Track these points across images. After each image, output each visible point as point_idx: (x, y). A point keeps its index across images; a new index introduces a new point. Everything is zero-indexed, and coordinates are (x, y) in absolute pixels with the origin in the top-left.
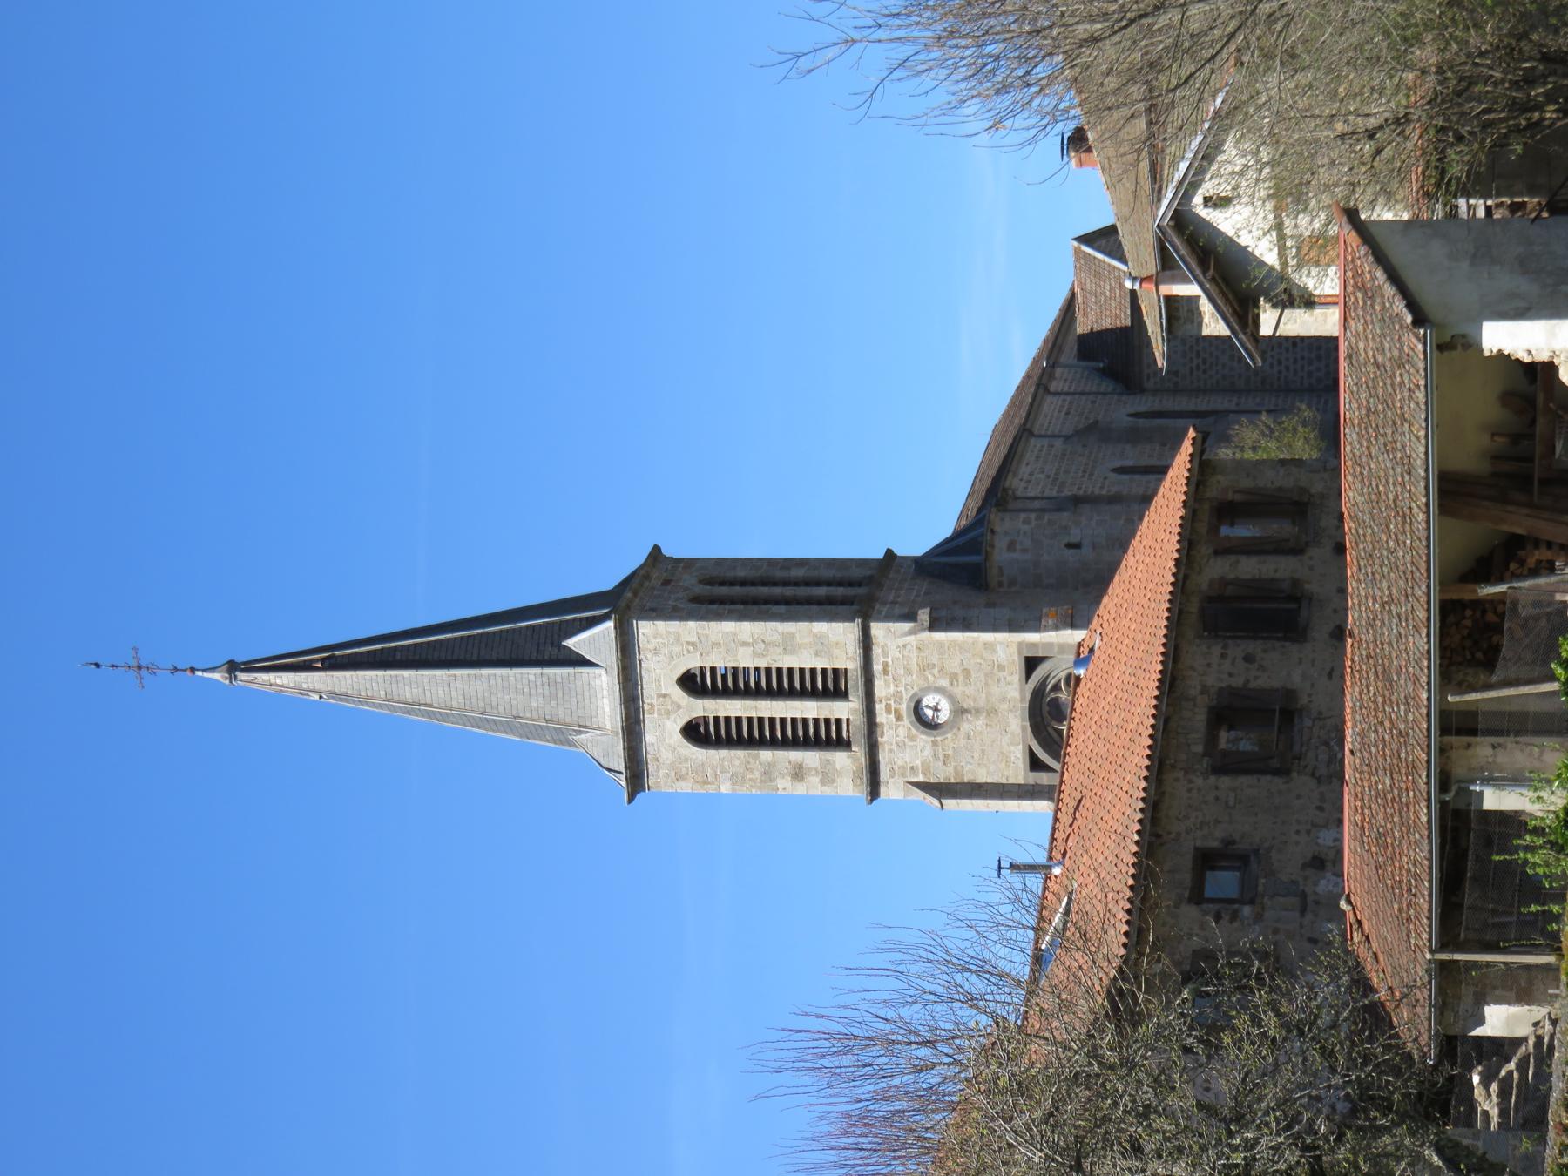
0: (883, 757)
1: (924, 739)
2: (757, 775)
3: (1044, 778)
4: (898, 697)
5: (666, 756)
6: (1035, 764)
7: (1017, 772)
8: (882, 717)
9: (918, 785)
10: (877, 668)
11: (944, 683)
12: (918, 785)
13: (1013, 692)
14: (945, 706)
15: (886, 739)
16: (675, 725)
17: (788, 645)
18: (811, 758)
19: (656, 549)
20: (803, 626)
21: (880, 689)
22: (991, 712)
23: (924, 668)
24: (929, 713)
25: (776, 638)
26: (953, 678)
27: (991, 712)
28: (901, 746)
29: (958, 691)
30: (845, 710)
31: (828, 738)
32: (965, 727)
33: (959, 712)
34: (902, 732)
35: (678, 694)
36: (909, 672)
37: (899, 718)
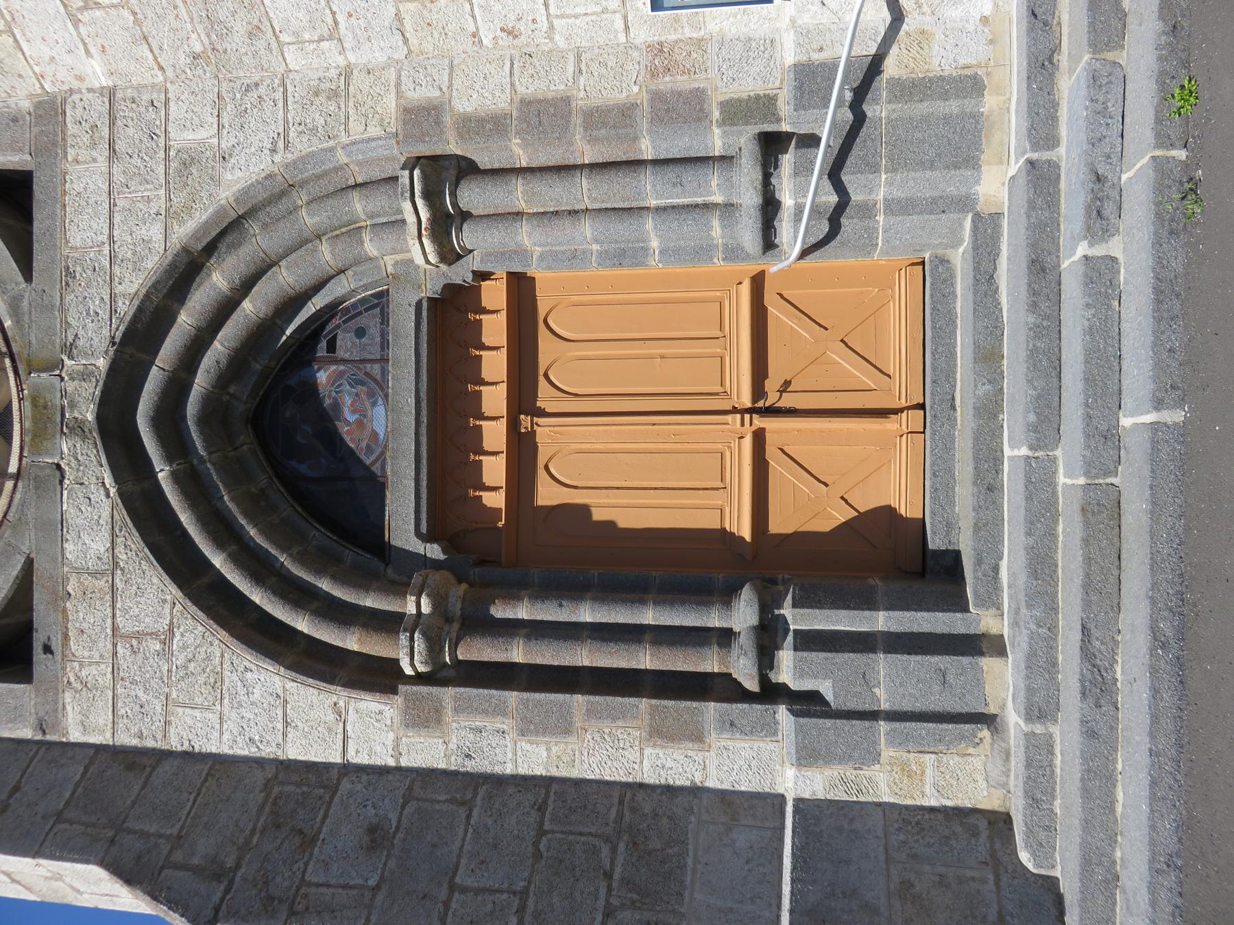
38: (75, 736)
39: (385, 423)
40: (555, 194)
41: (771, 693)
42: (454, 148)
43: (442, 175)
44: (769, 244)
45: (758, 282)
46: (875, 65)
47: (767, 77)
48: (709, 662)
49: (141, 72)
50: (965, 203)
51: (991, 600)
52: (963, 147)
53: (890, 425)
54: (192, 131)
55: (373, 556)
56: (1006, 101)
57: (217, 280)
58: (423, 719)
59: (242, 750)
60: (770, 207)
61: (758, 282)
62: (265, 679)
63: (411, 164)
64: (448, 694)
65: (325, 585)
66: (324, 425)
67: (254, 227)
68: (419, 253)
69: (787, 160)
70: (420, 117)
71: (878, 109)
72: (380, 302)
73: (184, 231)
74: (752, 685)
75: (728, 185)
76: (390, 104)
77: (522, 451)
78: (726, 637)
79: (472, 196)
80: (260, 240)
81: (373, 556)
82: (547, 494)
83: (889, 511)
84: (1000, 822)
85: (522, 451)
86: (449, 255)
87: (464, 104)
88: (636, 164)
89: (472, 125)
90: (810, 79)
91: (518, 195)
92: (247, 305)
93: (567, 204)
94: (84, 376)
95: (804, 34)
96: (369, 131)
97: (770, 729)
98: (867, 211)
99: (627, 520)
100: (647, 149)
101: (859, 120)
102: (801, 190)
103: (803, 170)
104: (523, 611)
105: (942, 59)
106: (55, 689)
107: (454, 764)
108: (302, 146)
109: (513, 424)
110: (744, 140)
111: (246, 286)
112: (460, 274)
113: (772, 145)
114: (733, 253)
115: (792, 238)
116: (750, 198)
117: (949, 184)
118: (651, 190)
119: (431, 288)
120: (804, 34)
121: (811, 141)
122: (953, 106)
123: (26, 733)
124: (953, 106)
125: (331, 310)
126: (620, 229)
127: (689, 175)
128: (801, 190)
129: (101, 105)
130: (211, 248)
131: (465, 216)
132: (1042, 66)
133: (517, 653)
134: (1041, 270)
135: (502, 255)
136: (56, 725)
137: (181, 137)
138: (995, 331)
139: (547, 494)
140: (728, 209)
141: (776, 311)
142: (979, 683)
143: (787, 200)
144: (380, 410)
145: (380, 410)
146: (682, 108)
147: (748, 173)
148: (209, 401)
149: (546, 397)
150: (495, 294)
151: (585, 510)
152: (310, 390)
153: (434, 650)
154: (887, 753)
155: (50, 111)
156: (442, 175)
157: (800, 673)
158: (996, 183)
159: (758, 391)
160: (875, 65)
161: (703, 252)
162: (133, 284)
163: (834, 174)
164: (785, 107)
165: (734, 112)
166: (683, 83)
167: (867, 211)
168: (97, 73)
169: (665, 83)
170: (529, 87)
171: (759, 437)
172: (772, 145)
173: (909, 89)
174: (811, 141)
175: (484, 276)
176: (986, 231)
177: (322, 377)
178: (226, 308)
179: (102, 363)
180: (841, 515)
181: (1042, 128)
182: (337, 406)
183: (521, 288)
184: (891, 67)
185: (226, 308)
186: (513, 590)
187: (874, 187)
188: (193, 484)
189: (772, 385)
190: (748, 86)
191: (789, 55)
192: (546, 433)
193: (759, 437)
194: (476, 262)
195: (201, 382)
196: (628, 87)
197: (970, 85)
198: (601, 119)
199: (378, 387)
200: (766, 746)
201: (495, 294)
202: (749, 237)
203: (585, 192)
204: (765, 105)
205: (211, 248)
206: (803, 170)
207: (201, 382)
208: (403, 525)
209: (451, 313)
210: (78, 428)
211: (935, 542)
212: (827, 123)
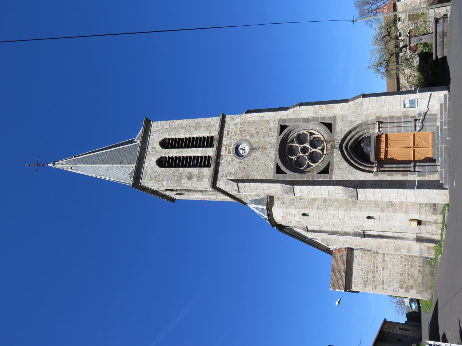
0: (221, 169)
1: (237, 160)
2: (176, 178)
3: (281, 177)
4: (230, 144)
5: (149, 171)
6: (279, 171)
7: (270, 174)
8: (223, 152)
9: (231, 180)
10: (225, 133)
11: (248, 137)
12: (231, 180)
13: (274, 140)
14: (247, 148)
15: (223, 162)
16: (154, 159)
17: (197, 127)
18: (195, 171)
19: (385, 319)
20: (203, 119)
21: (225, 142)
22: (264, 149)
23: (242, 131)
24: (241, 151)
25: (194, 125)
26: (252, 135)
27: (264, 149)
28: (228, 164)
29: (252, 141)
30: (210, 152)
31: (202, 162)
32: (253, 155)
33: (252, 149)
34: (229, 158)
35: (158, 147)
36: (236, 134)
37: (229, 153)
38: (334, 179)
39: (371, 150)
40: (392, 125)
41: (415, 171)
42: (381, 120)
43: (380, 123)
44: (415, 130)
45: (414, 135)
46: (426, 113)
47: (416, 114)
48: (408, 169)
49: (347, 113)
50: (436, 125)
51: (438, 162)
52: (435, 120)
53: (429, 148)
54: (352, 118)
55: (369, 162)
56: (439, 116)
57: (353, 133)
58: (376, 175)
59: (355, 180)
60: (415, 126)
61: (414, 135)
62: (358, 172)
63: (377, 122)
64: (379, 173)
65: (364, 164)
66: (362, 149)
67: (357, 128)
68: (377, 131)
69: (417, 122)
70: (378, 117)
71: (427, 117)
72: (370, 137)
73: (350, 128)
74: (413, 170)
75: (411, 124)
76: (375, 116)
77: (386, 152)
78: (410, 167)
79: (383, 125)
80: (358, 129)
81: (369, 162)
82: (389, 157)
83: (429, 157)
84: (439, 181)
85: (386, 152)
86: (379, 131)
87: (383, 116)
88: (401, 122)
89: (384, 118)
90: (420, 114)
91: (388, 125)
92: (356, 136)
93: (309, 175)
94: (338, 142)
95: (419, 110)
96: (372, 118)
97: (415, 174)
98: (426, 126)
99: (398, 159)
100: (402, 121)
101: (425, 118)
102: (419, 124)
103: (419, 122)
104: (387, 166)
105: (433, 112)
106: (332, 174)
107: (380, 180)
108: (365, 120)
109: (385, 149)
110: (413, 120)
111: (356, 134)
112: (380, 134)
113: (416, 120)
114: (411, 131)
115: (418, 129)
116: (413, 125)
117: (434, 124)
118: (403, 125)
119: (376, 135)
120: (419, 110)
121: (420, 120)
122: (434, 117)
123: (328, 179)
124: (434, 117)
125: (364, 137)
126: (399, 128)
127: (407, 123)
128: (419, 124)
129: (341, 116)
130: (352, 130)
131: (381, 127)
132: (441, 113)
133: (387, 169)
134: (441, 130)
135: (385, 132)
136: (332, 178)
137: (351, 119)
138: (439, 137)
139: (389, 157)
140: (411, 126)
141: (416, 137)
142: (437, 168)
143: (417, 125)
144: (369, 148)
145: (369, 148)
146: (407, 117)
147: (413, 123)
148: (350, 146)
149: (389, 146)
150: (384, 136)
151: (393, 158)
152: (361, 146)
153: (377, 169)
154: (427, 175)
155: (335, 117)
156: (380, 123)
157: (418, 169)
158: (438, 124)
159: (414, 145)
160: (426, 113)
161: (408, 131)
162: (344, 134)
163: (422, 123)
164: (417, 117)
165: (412, 117)
166: (406, 114)
167: (426, 126)
168: (342, 113)
169: (405, 114)
170: (390, 115)
171: (414, 150)
172: (416, 120)
173: (429, 115)
174: (420, 120)
175: (382, 134)
176: (438, 128)
177: (362, 145)
178: (354, 136)
179: (340, 141)
180: (423, 158)
181: (441, 118)
182: (364, 148)
183: (387, 135)
184: (428, 113)
185: (354, 136)
186: (386, 164)
187: (426, 124)
188: (348, 153)
189: (416, 145)
190: (413, 115)
191: (418, 112)
192: (389, 150)
193: (414, 150)
194: (382, 132)
195: (350, 144)
196: (401, 115)
197: (436, 115)
198: (397, 118)
199: (369, 145)
200: (414, 176)
201: (384, 136)
202: (413, 129)
203: (396, 125)
204: (415, 116)
205: (352, 130)
206: (419, 122)
207: (350, 144)
208: (372, 159)
209: (378, 138)
210: (336, 148)
211: (434, 159)
212: (421, 118)
